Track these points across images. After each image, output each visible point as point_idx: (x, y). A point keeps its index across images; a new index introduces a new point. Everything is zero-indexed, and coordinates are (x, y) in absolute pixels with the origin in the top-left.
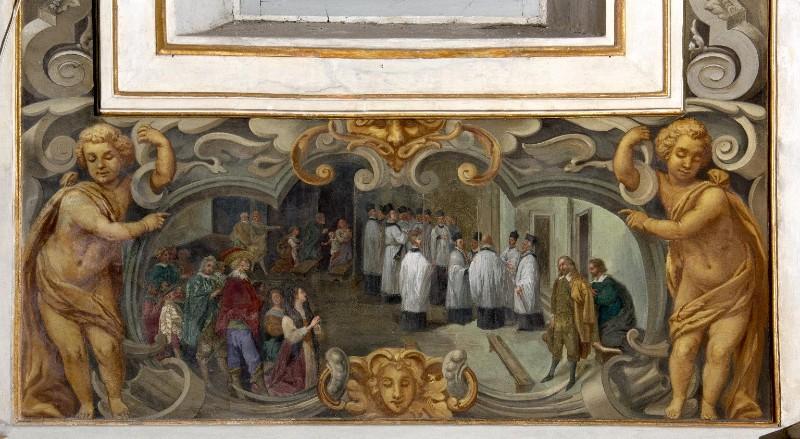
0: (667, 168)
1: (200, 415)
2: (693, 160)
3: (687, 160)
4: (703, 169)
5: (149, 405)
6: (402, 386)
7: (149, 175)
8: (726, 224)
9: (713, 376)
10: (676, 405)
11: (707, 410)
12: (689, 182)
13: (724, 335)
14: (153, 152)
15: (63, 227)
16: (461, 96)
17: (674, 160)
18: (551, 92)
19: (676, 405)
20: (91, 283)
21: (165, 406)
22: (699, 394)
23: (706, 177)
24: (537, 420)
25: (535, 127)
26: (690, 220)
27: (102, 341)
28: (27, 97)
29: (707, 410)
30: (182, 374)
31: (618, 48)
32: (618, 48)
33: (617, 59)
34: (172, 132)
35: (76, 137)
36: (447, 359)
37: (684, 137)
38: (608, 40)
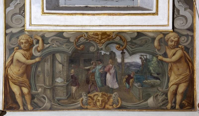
0: (168, 45)
1: (51, 109)
2: (175, 43)
3: (173, 43)
4: (177, 44)
5: (36, 107)
6: (102, 102)
7: (37, 48)
8: (183, 60)
9: (179, 98)
10: (169, 106)
11: (177, 107)
12: (174, 48)
13: (182, 89)
14: (38, 42)
15: (14, 61)
16: (114, 26)
17: (170, 43)
18: (148, 25)
19: (169, 106)
20: (22, 75)
21: (40, 107)
22: (175, 103)
23: (178, 47)
24: (133, 109)
25: (136, 34)
26: (175, 58)
27: (25, 90)
28: (7, 27)
29: (177, 107)
30: (45, 99)
31: (44, 13)
32: (44, 13)
33: (156, 17)
34: (43, 37)
35: (18, 38)
36: (113, 95)
37: (173, 36)
38: (45, 11)
